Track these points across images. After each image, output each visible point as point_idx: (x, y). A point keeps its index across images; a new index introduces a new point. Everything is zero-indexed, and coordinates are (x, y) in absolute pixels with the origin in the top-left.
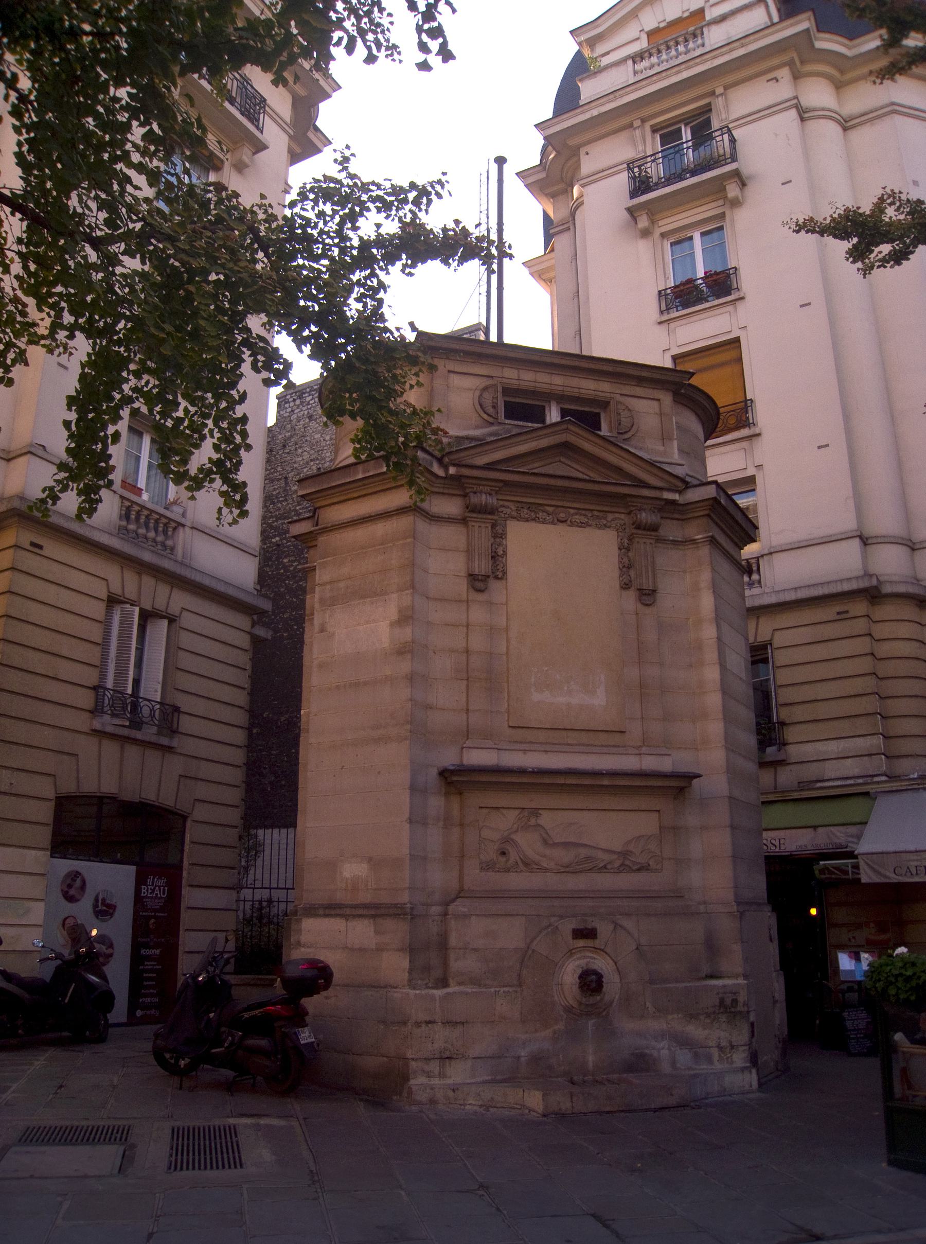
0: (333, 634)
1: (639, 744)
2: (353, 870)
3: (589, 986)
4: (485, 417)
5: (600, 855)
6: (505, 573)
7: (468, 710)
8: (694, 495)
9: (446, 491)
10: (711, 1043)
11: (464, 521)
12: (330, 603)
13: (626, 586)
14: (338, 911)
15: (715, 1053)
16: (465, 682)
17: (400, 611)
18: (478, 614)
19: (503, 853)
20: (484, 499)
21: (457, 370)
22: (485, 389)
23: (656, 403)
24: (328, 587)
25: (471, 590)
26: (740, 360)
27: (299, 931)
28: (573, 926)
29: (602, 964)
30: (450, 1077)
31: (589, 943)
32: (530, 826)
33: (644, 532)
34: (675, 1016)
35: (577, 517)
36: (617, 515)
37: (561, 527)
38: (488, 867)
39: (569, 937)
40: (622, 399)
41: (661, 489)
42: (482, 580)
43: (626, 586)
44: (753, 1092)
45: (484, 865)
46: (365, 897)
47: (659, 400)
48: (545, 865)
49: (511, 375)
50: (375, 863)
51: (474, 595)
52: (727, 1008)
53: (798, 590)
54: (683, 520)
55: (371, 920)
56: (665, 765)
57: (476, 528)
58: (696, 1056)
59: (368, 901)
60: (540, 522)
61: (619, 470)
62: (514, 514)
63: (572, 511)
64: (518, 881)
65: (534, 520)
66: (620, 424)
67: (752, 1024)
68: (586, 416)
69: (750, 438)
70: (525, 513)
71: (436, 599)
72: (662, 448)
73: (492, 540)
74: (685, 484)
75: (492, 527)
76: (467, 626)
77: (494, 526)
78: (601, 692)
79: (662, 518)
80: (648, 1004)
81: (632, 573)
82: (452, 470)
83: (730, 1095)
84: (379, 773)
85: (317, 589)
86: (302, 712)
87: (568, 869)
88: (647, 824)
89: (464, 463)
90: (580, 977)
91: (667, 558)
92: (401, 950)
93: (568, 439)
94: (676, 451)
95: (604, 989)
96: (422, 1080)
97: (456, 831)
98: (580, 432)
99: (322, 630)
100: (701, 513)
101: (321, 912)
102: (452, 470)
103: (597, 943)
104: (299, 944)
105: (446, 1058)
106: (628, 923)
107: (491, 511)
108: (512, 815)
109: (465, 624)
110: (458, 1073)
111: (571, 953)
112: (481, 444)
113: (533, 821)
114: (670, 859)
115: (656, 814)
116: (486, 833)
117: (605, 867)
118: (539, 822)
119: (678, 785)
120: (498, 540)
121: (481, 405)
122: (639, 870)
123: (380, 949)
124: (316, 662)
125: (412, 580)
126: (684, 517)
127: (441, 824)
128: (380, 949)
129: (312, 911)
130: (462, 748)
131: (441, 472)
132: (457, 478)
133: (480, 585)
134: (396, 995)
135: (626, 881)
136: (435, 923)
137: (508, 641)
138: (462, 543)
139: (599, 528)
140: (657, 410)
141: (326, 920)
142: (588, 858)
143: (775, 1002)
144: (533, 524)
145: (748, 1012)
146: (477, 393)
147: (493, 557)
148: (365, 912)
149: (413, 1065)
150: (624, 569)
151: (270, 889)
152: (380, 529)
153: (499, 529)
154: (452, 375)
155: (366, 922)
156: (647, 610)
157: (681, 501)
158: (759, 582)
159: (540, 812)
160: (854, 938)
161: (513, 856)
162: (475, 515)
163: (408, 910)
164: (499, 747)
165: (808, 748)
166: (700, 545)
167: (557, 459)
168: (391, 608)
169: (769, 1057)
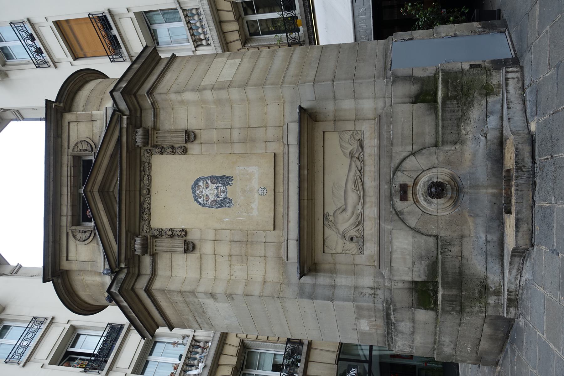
1: (282, 144)
4: (91, 238)
5: (352, 174)
8: (123, 106)
9: (137, 265)
11: (154, 256)
13: (185, 151)
18: (207, 248)
19: (352, 239)
21: (65, 255)
22: (75, 237)
26: (67, 21)
28: (398, 200)
33: (150, 139)
36: (142, 155)
39: (406, 203)
40: (71, 148)
41: (121, 129)
42: (188, 246)
43: (185, 151)
45: (360, 251)
47: (69, 123)
49: (65, 221)
50: (359, 317)
54: (141, 110)
56: (294, 127)
57: (157, 248)
61: (113, 156)
62: (147, 223)
63: (142, 185)
64: (370, 228)
65: (149, 210)
68: (84, 168)
69: (112, 16)
70: (146, 216)
72: (99, 122)
77: (155, 237)
78: (251, 169)
81: (176, 146)
88: (333, 140)
91: (166, 123)
98: (92, 180)
100: (134, 99)
102: (123, 266)
107: (145, 239)
108: (328, 231)
111: (416, 202)
113: (331, 218)
114: (355, 125)
115: (326, 133)
117: (360, 171)
118: (332, 214)
119: (308, 118)
121: (85, 241)
122: (362, 147)
126: (138, 108)
133: (191, 246)
136: (396, 284)
138: (168, 256)
139: (151, 167)
140: (76, 123)
142: (355, 184)
146: (78, 242)
153: (156, 233)
154: (69, 258)
157: (127, 113)
158: (197, 9)
159: (325, 213)
162: (149, 250)
164: (286, 239)
167: (111, 194)
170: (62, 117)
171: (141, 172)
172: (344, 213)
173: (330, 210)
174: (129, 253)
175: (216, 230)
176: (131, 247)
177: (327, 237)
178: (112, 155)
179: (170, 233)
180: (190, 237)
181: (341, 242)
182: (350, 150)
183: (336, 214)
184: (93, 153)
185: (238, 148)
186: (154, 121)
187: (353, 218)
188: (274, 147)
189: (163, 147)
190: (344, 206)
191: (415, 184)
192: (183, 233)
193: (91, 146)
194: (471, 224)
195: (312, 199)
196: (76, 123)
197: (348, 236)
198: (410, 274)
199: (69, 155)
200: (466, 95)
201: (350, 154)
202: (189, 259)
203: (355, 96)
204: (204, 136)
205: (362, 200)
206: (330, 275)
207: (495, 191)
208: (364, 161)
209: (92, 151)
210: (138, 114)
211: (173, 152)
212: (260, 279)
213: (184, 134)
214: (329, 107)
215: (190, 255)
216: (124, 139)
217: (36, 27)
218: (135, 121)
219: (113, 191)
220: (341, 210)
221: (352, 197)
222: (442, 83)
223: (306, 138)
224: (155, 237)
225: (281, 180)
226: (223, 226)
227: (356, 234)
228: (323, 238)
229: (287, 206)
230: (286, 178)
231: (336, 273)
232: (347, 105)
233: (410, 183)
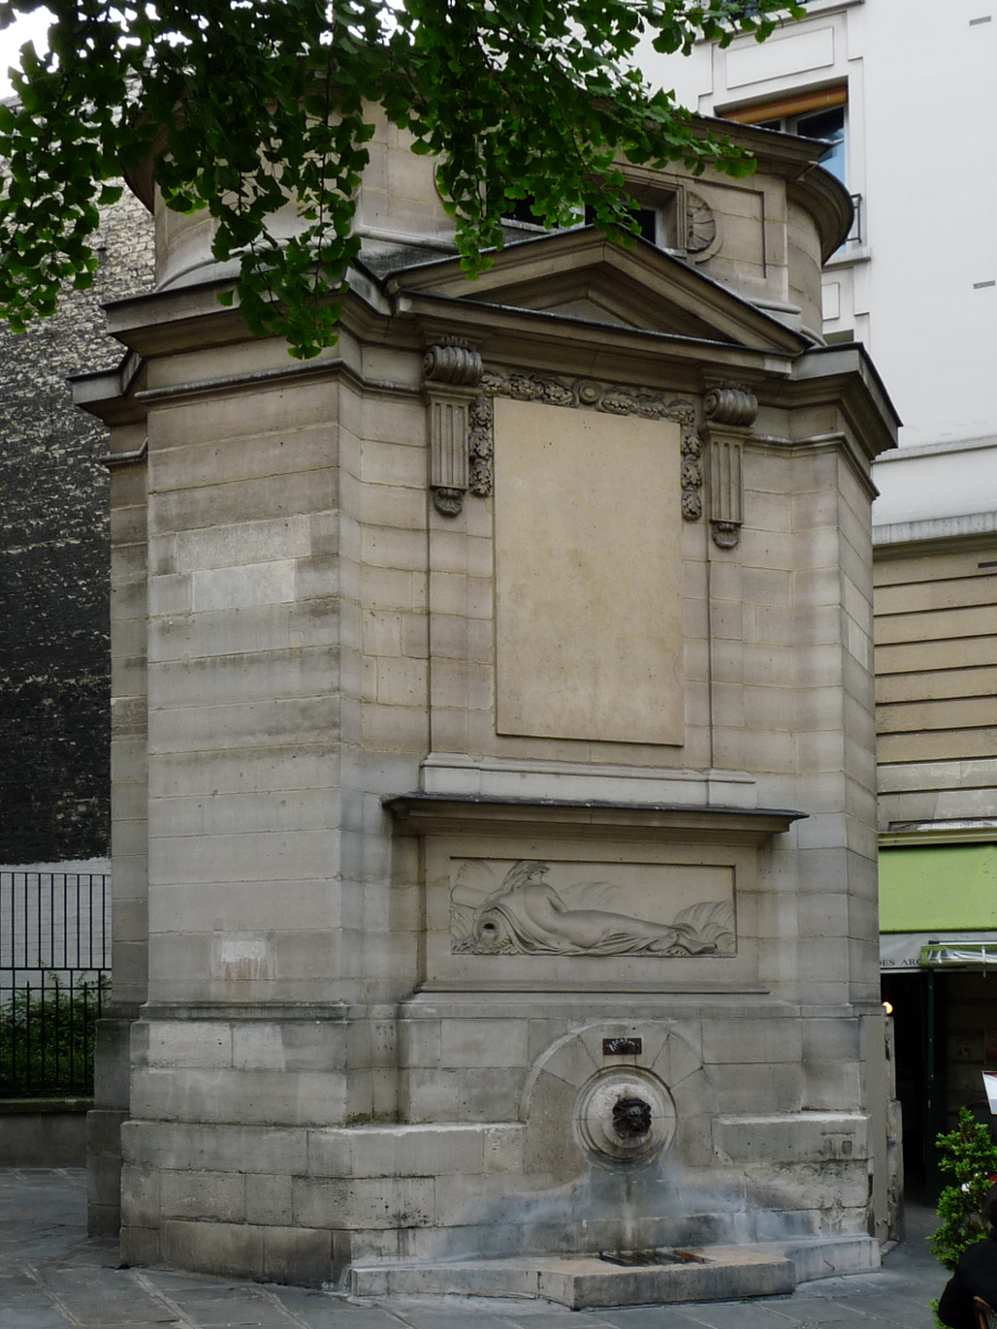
0: (186, 580)
2: (233, 951)
3: (629, 1122)
5: (639, 929)
6: (491, 487)
7: (430, 707)
8: (817, 367)
9: (388, 341)
10: (808, 1203)
11: (421, 397)
12: (182, 524)
13: (690, 516)
14: (214, 1013)
15: (816, 1216)
16: (425, 663)
17: (315, 543)
18: (445, 553)
19: (490, 927)
20: (462, 358)
23: (755, 200)
24: (174, 497)
25: (433, 513)
27: (146, 1043)
29: (641, 1090)
30: (415, 1255)
31: (629, 1060)
32: (532, 886)
33: (728, 428)
34: (757, 1165)
35: (615, 396)
36: (681, 396)
37: (588, 415)
38: (465, 947)
42: (453, 498)
43: (690, 516)
44: (873, 1272)
45: (459, 944)
46: (261, 992)
47: (760, 194)
48: (555, 945)
50: (280, 941)
51: (437, 522)
52: (832, 1158)
53: (894, 528)
55: (278, 1028)
57: (444, 408)
58: (789, 1221)
59: (268, 998)
60: (549, 403)
61: (692, 321)
62: (507, 385)
64: (513, 967)
65: (541, 398)
66: (691, 234)
67: (870, 1177)
70: (526, 386)
71: (372, 526)
72: (762, 281)
73: (469, 430)
74: (801, 345)
75: (470, 408)
76: (428, 572)
77: (473, 406)
79: (759, 404)
80: (716, 1148)
82: (404, 306)
83: (841, 1276)
84: (284, 802)
85: (152, 500)
86: (113, 701)
87: (590, 951)
88: (711, 886)
89: (425, 292)
90: (616, 1109)
91: (760, 472)
92: (333, 1070)
93: (607, 259)
94: (786, 287)
95: (652, 1127)
96: (372, 1259)
97: (412, 893)
99: (166, 569)
100: (826, 398)
101: (184, 1014)
102: (404, 306)
103: (641, 1060)
104: (144, 1062)
105: (404, 1226)
106: (688, 1033)
108: (503, 869)
109: (424, 568)
110: (423, 1251)
111: (600, 1075)
112: (448, 260)
113: (536, 879)
114: (749, 938)
115: (729, 873)
116: (460, 896)
117: (648, 948)
119: (762, 832)
120: (479, 430)
123: (293, 1069)
124: (154, 624)
125: (337, 493)
126: (796, 403)
127: (387, 882)
128: (293, 1069)
129: (165, 1013)
130: (422, 767)
131: (384, 309)
132: (414, 319)
133: (448, 506)
134: (324, 1138)
135: (681, 970)
136: (381, 1030)
137: (495, 598)
139: (650, 417)
140: (757, 211)
141: (196, 1026)
142: (620, 936)
143: (890, 1144)
144: (536, 406)
145: (866, 1160)
147: (472, 460)
148: (265, 1014)
149: (356, 1239)
150: (690, 488)
151: (14, 969)
152: (272, 402)
153: (482, 411)
155: (268, 1029)
156: (725, 556)
159: (547, 865)
160: (967, 1050)
161: (505, 930)
162: (441, 386)
163: (344, 1013)
164: (481, 765)
165: (912, 772)
166: (819, 452)
167: (582, 293)
168: (299, 537)
169: (884, 1216)
170: (776, 176)
171: (638, 386)
172: (550, 909)
173: (556, 876)
174: (435, 326)
175: (494, 579)
176: (451, 334)
177: (491, 871)
178: (695, 317)
179: (484, 452)
180: (470, 503)
181: (477, 900)
182: (693, 926)
183: (549, 891)
184: (686, 255)
185: (695, 655)
186: (765, 442)
187: (542, 931)
188: (697, 743)
189: (698, 457)
190: (564, 911)
191: (639, 1071)
192: (483, 489)
193: (701, 250)
194: (558, 1191)
195: (584, 833)
196: (759, 216)
197: (495, 918)
198: (426, 1062)
199: (681, 181)
200: (822, 1169)
201: (685, 925)
202: (410, 495)
203: (808, 939)
204: (725, 568)
205: (582, 952)
206: (389, 871)
207: (629, 1235)
208: (672, 956)
209: (689, 251)
210: (779, 401)
211: (690, 483)
212: (370, 689)
213: (733, 520)
214: (783, 879)
215: (421, 500)
216: (737, 360)
217: (834, 21)
218: (779, 394)
219: (587, 297)
220: (556, 902)
221: (592, 931)
222: (847, 1121)
223: (730, 827)
224: (473, 406)
225: (620, 760)
226: (504, 602)
227: (503, 937)
228: (489, 859)
229: (561, 770)
230: (627, 774)
231: (394, 886)
232: (787, 921)
233: (642, 1060)
